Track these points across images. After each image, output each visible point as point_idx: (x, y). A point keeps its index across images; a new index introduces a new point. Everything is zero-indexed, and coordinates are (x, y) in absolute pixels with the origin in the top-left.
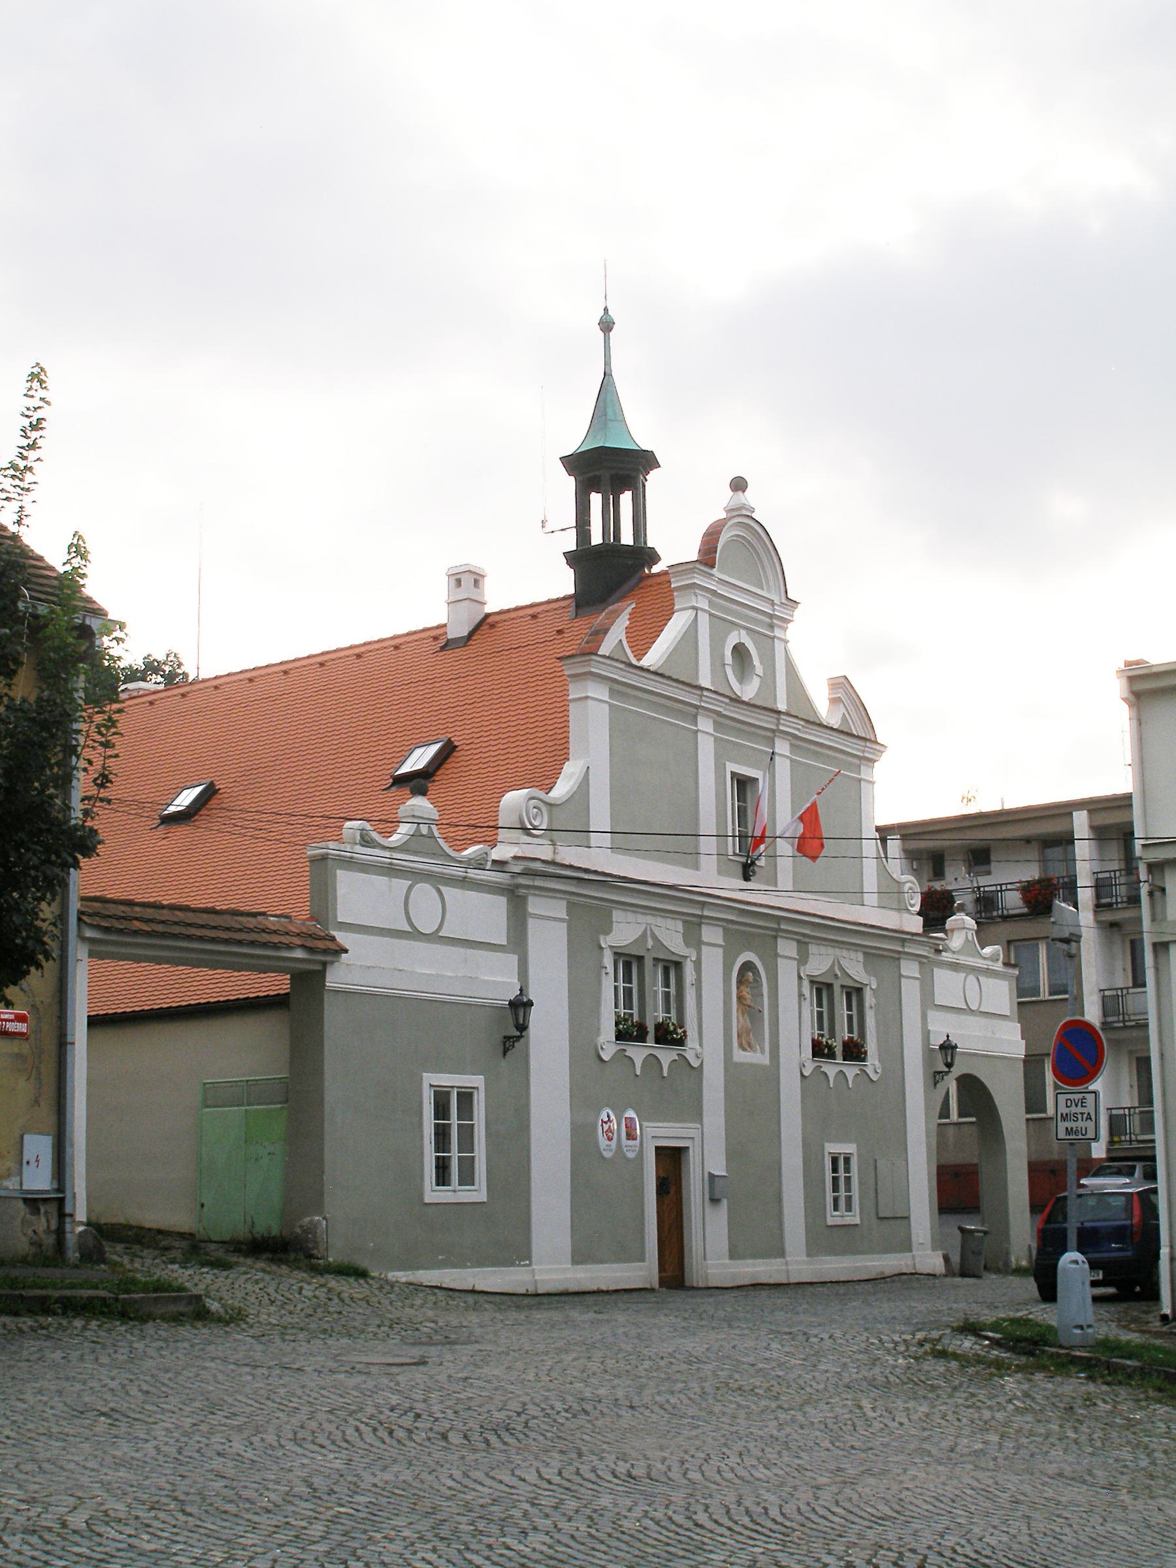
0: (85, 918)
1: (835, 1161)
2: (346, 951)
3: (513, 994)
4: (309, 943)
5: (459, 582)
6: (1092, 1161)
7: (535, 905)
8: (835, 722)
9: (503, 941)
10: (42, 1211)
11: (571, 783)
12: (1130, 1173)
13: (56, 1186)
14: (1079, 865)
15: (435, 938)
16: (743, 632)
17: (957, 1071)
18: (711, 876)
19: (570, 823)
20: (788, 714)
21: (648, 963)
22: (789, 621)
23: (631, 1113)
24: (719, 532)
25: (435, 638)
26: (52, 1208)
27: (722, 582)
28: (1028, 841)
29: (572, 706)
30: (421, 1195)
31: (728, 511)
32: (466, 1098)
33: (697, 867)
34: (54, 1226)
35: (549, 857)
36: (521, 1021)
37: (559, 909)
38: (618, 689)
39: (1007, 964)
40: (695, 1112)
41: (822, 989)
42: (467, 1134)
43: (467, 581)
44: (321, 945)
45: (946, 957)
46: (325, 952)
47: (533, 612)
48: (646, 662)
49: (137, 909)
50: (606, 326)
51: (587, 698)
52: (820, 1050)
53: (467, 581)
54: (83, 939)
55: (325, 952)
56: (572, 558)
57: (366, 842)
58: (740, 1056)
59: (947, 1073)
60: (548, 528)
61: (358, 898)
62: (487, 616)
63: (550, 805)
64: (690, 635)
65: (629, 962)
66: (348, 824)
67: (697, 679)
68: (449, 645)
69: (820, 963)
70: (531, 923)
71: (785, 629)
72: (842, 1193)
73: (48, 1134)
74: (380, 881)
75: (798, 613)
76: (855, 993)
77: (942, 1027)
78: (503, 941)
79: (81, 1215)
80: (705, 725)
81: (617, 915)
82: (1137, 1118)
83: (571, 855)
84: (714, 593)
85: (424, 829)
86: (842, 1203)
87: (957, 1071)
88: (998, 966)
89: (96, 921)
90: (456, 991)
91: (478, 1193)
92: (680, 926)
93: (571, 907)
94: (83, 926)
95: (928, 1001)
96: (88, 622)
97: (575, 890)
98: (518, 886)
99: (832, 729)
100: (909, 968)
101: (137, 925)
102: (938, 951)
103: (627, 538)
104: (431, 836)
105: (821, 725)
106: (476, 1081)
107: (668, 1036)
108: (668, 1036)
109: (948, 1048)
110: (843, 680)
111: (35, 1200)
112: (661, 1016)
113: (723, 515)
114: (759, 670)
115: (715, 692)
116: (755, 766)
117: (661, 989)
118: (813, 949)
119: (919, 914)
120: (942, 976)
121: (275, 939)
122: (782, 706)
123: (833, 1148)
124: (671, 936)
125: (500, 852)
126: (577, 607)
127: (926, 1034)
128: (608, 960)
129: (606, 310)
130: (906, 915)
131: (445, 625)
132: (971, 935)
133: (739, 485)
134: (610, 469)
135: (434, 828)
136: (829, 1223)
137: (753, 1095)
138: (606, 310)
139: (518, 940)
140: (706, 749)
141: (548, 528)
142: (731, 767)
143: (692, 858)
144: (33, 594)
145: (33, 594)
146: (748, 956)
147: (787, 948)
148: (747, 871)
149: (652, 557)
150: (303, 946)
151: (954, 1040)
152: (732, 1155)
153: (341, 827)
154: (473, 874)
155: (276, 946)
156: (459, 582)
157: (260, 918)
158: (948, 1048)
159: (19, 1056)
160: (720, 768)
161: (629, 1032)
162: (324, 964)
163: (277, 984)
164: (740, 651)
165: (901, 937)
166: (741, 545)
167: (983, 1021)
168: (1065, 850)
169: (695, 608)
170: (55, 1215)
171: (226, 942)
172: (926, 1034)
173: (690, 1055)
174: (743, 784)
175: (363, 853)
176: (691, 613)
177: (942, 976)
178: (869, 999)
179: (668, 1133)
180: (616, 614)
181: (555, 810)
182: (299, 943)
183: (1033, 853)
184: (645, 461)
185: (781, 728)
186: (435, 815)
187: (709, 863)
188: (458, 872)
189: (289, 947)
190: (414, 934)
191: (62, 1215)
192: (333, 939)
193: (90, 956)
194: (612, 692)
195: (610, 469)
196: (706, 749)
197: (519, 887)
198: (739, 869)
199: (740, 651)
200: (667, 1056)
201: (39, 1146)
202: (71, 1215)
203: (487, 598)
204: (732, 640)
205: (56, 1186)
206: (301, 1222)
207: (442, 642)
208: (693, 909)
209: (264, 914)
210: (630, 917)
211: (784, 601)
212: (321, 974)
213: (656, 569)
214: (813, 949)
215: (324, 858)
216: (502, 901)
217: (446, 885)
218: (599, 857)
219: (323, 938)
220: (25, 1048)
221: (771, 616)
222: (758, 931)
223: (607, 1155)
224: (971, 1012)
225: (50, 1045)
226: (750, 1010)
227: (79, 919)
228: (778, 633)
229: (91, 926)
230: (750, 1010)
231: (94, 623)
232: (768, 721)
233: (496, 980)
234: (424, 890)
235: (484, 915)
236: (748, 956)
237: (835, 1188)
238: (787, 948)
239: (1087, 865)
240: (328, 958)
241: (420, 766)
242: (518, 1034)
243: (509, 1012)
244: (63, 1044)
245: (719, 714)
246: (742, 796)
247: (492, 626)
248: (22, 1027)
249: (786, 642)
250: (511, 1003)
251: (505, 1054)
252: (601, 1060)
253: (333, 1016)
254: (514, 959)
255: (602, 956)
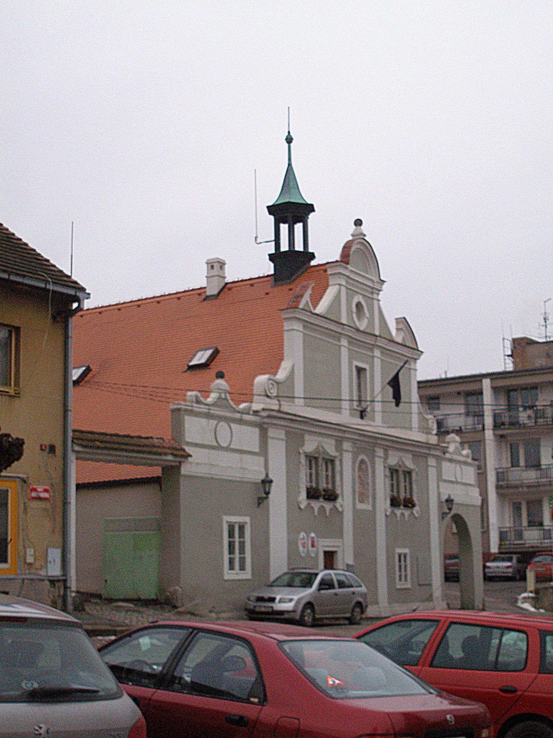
0: (75, 441)
1: (400, 557)
2: (191, 456)
3: (263, 477)
4: (175, 452)
5: (212, 267)
6: (491, 554)
7: (271, 432)
8: (399, 340)
9: (257, 450)
10: (57, 585)
11: (287, 372)
12: (510, 560)
13: (62, 573)
14: (485, 407)
15: (228, 449)
16: (361, 296)
17: (453, 512)
18: (345, 417)
19: (285, 391)
20: (380, 336)
21: (320, 460)
22: (380, 290)
23: (313, 535)
24: (350, 247)
25: (199, 294)
26: (61, 584)
27: (352, 271)
28: (459, 393)
29: (285, 333)
30: (222, 575)
31: (352, 235)
32: (242, 528)
33: (340, 413)
34: (62, 593)
35: (276, 408)
36: (267, 490)
37: (281, 434)
38: (307, 325)
39: (473, 459)
40: (340, 535)
41: (393, 472)
42: (242, 545)
43: (217, 266)
44: (180, 453)
45: (447, 456)
46: (182, 456)
47: (251, 282)
48: (318, 310)
49: (108, 437)
50: (289, 140)
51: (293, 330)
52: (394, 503)
53: (217, 266)
54: (73, 451)
55: (182, 456)
56: (272, 257)
57: (198, 402)
58: (359, 506)
59: (448, 513)
60: (258, 242)
61: (195, 429)
62: (226, 284)
63: (278, 383)
64: (338, 297)
65: (312, 459)
66: (189, 393)
67: (340, 319)
68: (207, 298)
69: (393, 461)
70: (270, 441)
71: (378, 294)
72: (237, 555)
73: (58, 547)
74: (204, 421)
75: (385, 286)
76: (408, 473)
77: (446, 491)
78: (257, 450)
79: (74, 589)
80: (344, 342)
81: (307, 437)
82: (513, 533)
83: (286, 407)
84: (348, 277)
85: (223, 396)
86: (403, 578)
87: (453, 512)
88: (470, 460)
89: (80, 442)
90: (237, 475)
91: (247, 575)
92: (333, 442)
93: (287, 433)
94: (74, 444)
95: (439, 478)
96: (78, 294)
97: (289, 425)
98: (264, 423)
99: (397, 343)
100: (432, 462)
101: (98, 443)
102: (444, 453)
103: (299, 247)
104: (226, 399)
105: (394, 342)
106: (247, 519)
107: (331, 496)
108: (331, 496)
109: (449, 501)
110: (403, 320)
111: (54, 581)
112: (325, 486)
113: (351, 238)
114: (367, 315)
115: (349, 326)
116: (366, 363)
117: (324, 473)
118: (390, 452)
119: (436, 435)
120: (446, 465)
121: (160, 450)
122: (377, 333)
123: (399, 550)
124: (331, 449)
125: (256, 406)
126: (275, 281)
127: (439, 494)
128: (303, 459)
129: (289, 132)
130: (430, 436)
131: (205, 288)
132: (458, 445)
133: (358, 223)
134: (291, 211)
135: (228, 395)
136: (399, 587)
137: (365, 524)
138: (289, 132)
139: (264, 451)
140: (344, 353)
141: (258, 242)
142: (356, 363)
143: (339, 410)
144: (53, 280)
145: (54, 281)
146: (362, 457)
147: (380, 452)
148: (362, 414)
149: (312, 256)
150: (172, 454)
151: (452, 497)
152: (356, 557)
153: (185, 395)
154: (246, 417)
155: (160, 454)
156: (212, 267)
157: (150, 440)
158: (449, 501)
159: (45, 509)
160: (350, 363)
161: (312, 494)
162: (180, 462)
163: (157, 472)
164: (359, 305)
165: (428, 446)
166: (358, 252)
167: (463, 487)
168: (478, 399)
169: (340, 285)
170: (63, 587)
171: (138, 452)
172: (439, 494)
173: (338, 505)
174: (360, 371)
175: (197, 408)
176: (338, 286)
177: (446, 465)
178: (414, 475)
179: (326, 544)
180: (305, 288)
181: (280, 385)
182: (170, 452)
183: (462, 400)
184: (310, 208)
185: (378, 343)
186: (228, 388)
187: (346, 413)
188: (238, 416)
189: (166, 454)
190: (219, 448)
191: (66, 588)
192: (184, 450)
193: (77, 459)
194: (304, 327)
195: (291, 211)
196: (344, 353)
197: (264, 424)
198: (358, 414)
199: (359, 305)
200: (328, 506)
201: (55, 554)
202: (70, 588)
203: (226, 275)
204: (357, 298)
205: (62, 573)
206: (170, 589)
207: (203, 297)
208: (339, 432)
209: (152, 438)
210: (312, 438)
211: (379, 281)
212: (178, 468)
213: (313, 263)
214: (390, 452)
215: (179, 410)
216: (257, 430)
217: (234, 423)
218: (299, 408)
219: (179, 450)
220: (48, 505)
221: (373, 288)
222: (369, 443)
223: (303, 555)
224: (457, 483)
225: (59, 503)
226: (363, 483)
227: (72, 441)
228: (375, 296)
229: (78, 445)
230: (363, 483)
231: (80, 294)
232: (371, 340)
233: (254, 470)
234: (223, 424)
235: (249, 437)
236: (362, 457)
237: (231, 551)
238: (380, 452)
239: (489, 407)
240: (183, 460)
241: (203, 361)
242: (265, 495)
243: (261, 485)
244: (65, 503)
245: (350, 337)
246: (359, 378)
247: (230, 289)
248: (46, 495)
249: (379, 300)
250: (263, 482)
251: (259, 504)
252: (300, 508)
253: (184, 488)
254: (262, 459)
255: (300, 458)
